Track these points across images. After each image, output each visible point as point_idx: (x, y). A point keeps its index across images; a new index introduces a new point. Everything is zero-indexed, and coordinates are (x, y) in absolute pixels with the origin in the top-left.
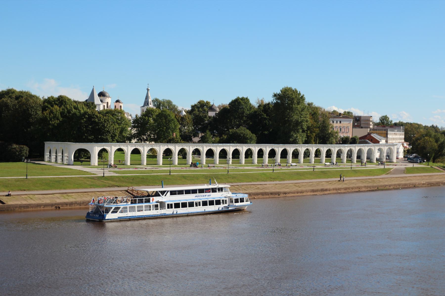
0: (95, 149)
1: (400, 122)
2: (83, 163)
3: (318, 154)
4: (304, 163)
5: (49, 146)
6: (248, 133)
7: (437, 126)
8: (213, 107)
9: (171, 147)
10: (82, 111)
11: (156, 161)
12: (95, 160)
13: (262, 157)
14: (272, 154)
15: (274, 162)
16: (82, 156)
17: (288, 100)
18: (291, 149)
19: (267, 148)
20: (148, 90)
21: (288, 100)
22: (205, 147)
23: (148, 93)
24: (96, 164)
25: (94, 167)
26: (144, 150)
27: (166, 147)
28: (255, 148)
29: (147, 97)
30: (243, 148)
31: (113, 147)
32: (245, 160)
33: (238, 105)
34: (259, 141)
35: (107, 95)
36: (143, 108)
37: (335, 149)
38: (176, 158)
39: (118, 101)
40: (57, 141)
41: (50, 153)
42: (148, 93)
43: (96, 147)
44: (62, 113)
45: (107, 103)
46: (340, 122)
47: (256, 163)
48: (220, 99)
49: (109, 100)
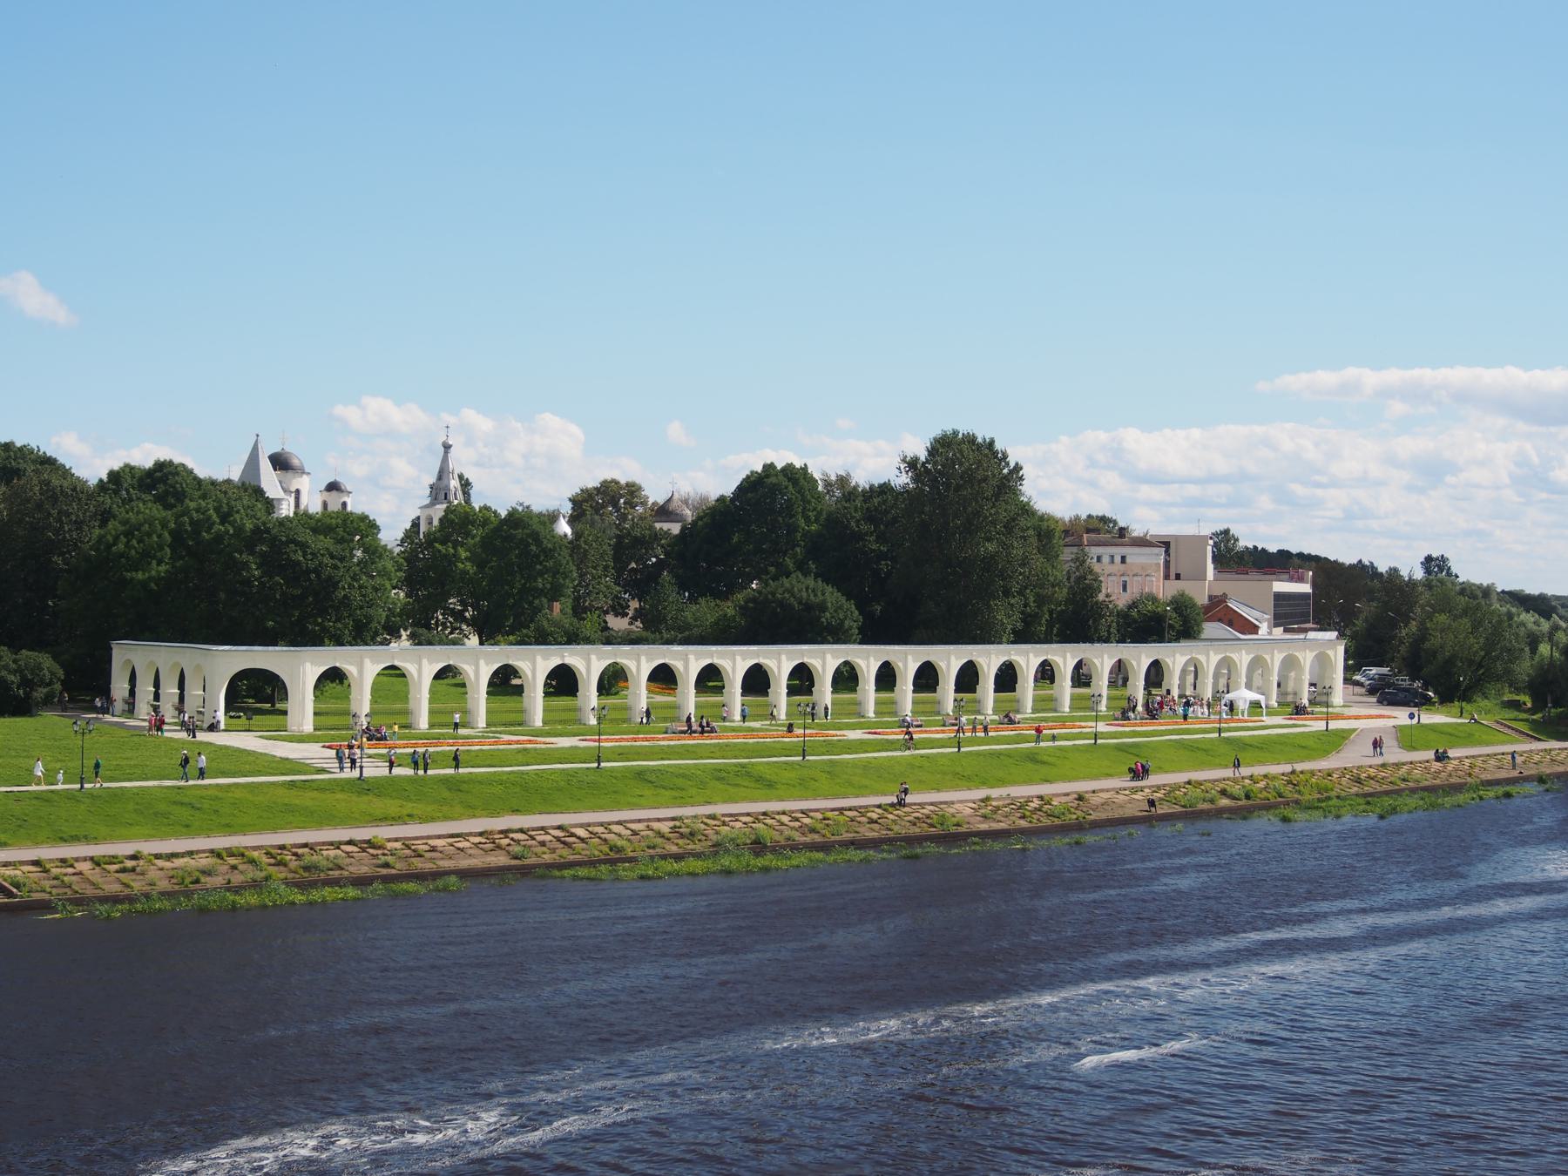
0: (301, 669)
1: (805, 469)
2: (257, 719)
3: (887, 678)
4: (1034, 711)
5: (127, 656)
6: (831, 596)
7: (805, 469)
8: (672, 506)
9: (572, 657)
10: (249, 526)
11: (522, 711)
12: (302, 707)
13: (767, 694)
14: (927, 678)
15: (519, 722)
16: (257, 695)
17: (964, 478)
18: (989, 659)
19: (908, 660)
20: (447, 447)
21: (964, 478)
22: (539, 659)
23: (445, 460)
24: (308, 727)
25: (297, 743)
26: (534, 672)
27: (555, 662)
28: (868, 660)
29: (255, 448)
30: (825, 660)
31: (539, 659)
32: (995, 701)
33: (770, 497)
34: (873, 634)
35: (295, 462)
36: (430, 511)
37: (1102, 658)
38: (536, 702)
39: (333, 487)
40: (305, 645)
41: (157, 685)
42: (445, 460)
43: (308, 665)
44: (177, 535)
45: (298, 492)
46: (1123, 559)
47: (872, 714)
48: (692, 471)
49: (302, 483)
